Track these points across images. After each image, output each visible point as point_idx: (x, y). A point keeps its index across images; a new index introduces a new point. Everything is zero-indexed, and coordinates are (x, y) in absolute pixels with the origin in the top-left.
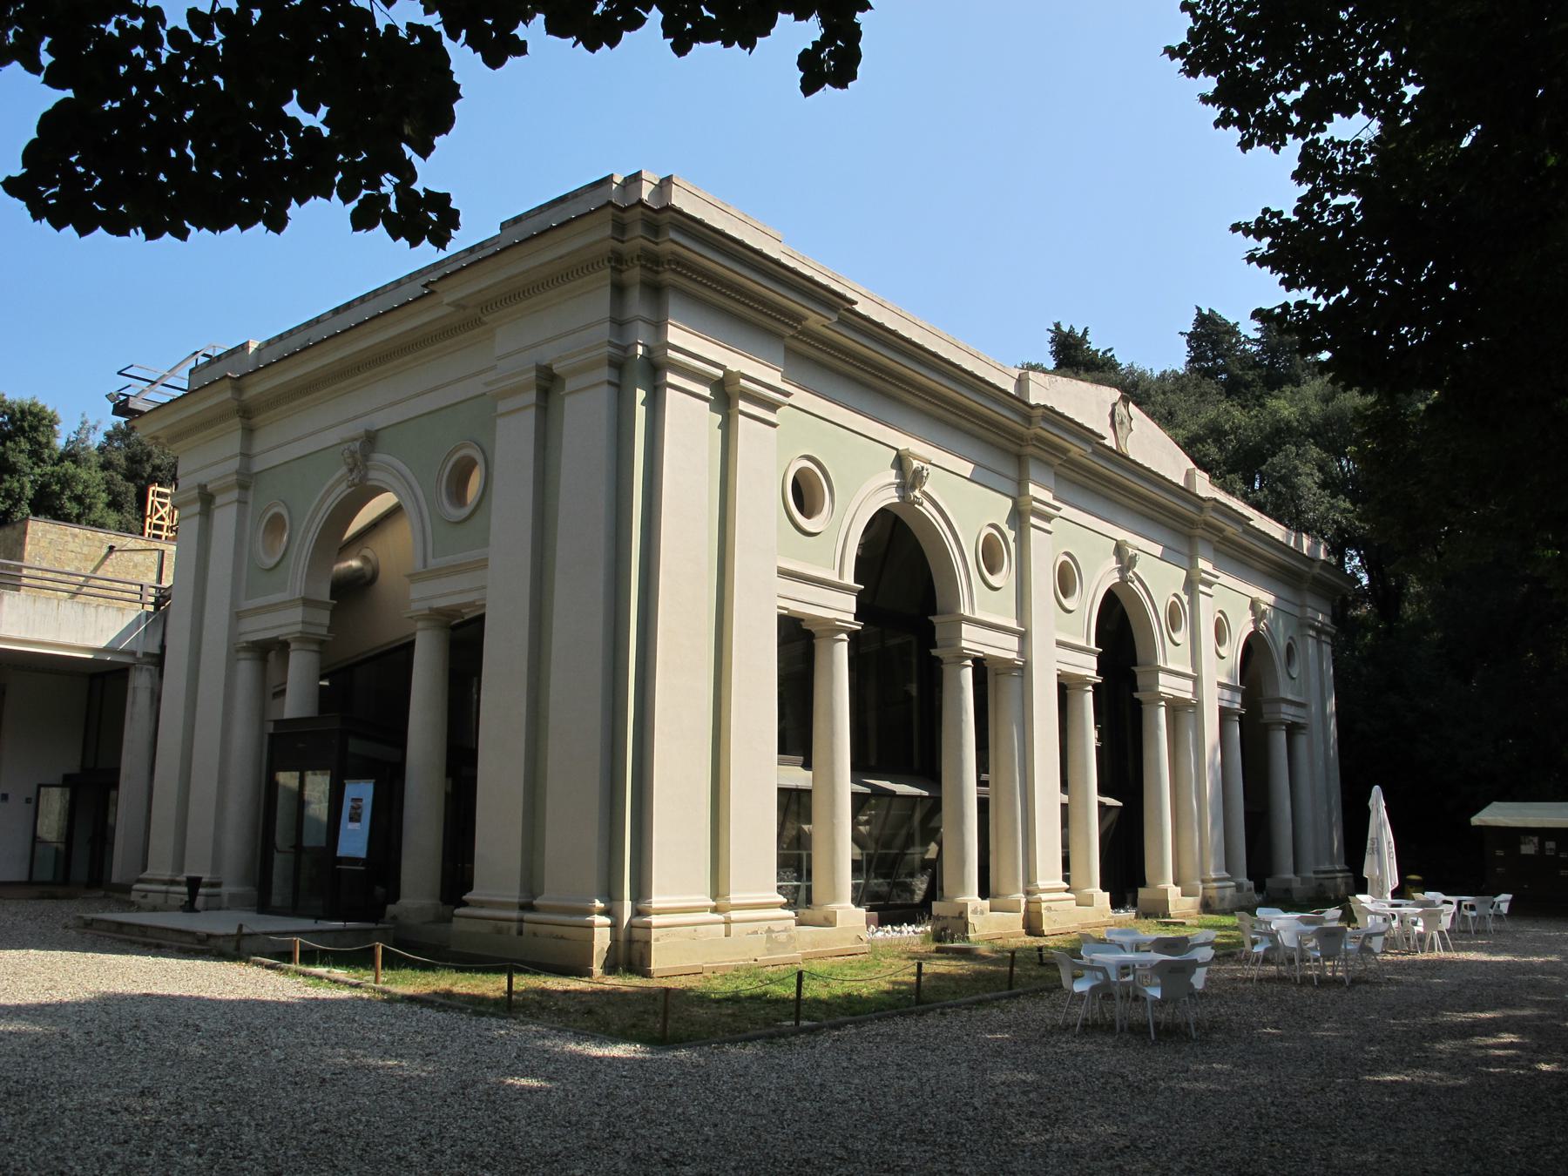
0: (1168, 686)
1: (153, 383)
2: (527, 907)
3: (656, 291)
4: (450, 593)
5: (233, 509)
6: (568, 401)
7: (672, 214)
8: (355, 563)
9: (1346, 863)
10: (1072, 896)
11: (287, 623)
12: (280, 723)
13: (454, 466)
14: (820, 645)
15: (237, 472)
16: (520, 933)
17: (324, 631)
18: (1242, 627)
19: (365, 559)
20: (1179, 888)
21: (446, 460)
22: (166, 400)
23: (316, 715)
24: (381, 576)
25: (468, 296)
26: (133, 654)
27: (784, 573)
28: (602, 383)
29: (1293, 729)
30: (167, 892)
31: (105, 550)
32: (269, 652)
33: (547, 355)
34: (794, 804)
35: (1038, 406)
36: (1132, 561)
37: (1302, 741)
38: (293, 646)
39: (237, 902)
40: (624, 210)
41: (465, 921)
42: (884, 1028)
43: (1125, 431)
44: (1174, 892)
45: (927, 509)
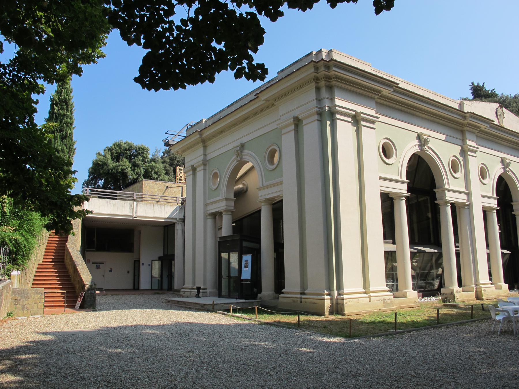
1: (175, 135)
2: (303, 293)
3: (330, 88)
4: (272, 193)
6: (304, 127)
8: (241, 186)
11: (221, 206)
14: (396, 202)
17: (233, 208)
19: (244, 184)
23: (232, 235)
26: (176, 219)
27: (381, 178)
30: (191, 292)
32: (216, 216)
33: (296, 113)
35: (468, 113)
38: (223, 213)
39: (212, 294)
41: (283, 299)
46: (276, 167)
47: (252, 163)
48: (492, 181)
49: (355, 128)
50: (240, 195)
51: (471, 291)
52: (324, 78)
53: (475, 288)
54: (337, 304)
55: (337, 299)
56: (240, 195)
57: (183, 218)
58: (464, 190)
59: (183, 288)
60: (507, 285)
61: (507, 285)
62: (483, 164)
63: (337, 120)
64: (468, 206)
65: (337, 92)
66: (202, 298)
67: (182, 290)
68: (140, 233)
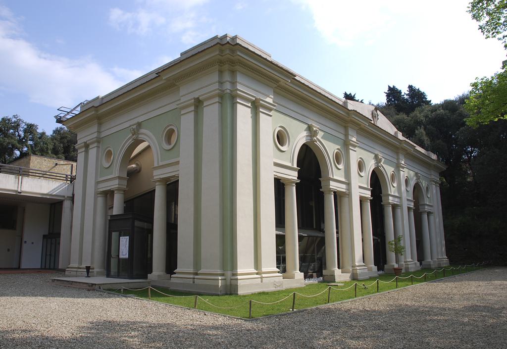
1: (68, 113)
2: (197, 274)
3: (233, 73)
5: (95, 149)
6: (205, 109)
8: (134, 166)
11: (114, 185)
12: (112, 216)
13: (169, 129)
15: (96, 137)
16: (194, 282)
17: (125, 187)
19: (137, 164)
20: (340, 270)
21: (166, 128)
24: (142, 169)
26: (64, 196)
27: (276, 164)
28: (216, 102)
29: (429, 213)
30: (77, 271)
31: (54, 165)
32: (108, 195)
34: (281, 240)
35: (351, 110)
37: (432, 217)
38: (115, 192)
39: (99, 274)
40: (223, 45)
41: (176, 280)
42: (284, 313)
43: (377, 119)
44: (338, 272)
47: (148, 141)
50: (133, 175)
57: (72, 196)
58: (343, 180)
59: (68, 268)
60: (376, 267)
62: (360, 158)
64: (348, 195)
65: (240, 78)
66: (25, 121)
68: (24, 210)
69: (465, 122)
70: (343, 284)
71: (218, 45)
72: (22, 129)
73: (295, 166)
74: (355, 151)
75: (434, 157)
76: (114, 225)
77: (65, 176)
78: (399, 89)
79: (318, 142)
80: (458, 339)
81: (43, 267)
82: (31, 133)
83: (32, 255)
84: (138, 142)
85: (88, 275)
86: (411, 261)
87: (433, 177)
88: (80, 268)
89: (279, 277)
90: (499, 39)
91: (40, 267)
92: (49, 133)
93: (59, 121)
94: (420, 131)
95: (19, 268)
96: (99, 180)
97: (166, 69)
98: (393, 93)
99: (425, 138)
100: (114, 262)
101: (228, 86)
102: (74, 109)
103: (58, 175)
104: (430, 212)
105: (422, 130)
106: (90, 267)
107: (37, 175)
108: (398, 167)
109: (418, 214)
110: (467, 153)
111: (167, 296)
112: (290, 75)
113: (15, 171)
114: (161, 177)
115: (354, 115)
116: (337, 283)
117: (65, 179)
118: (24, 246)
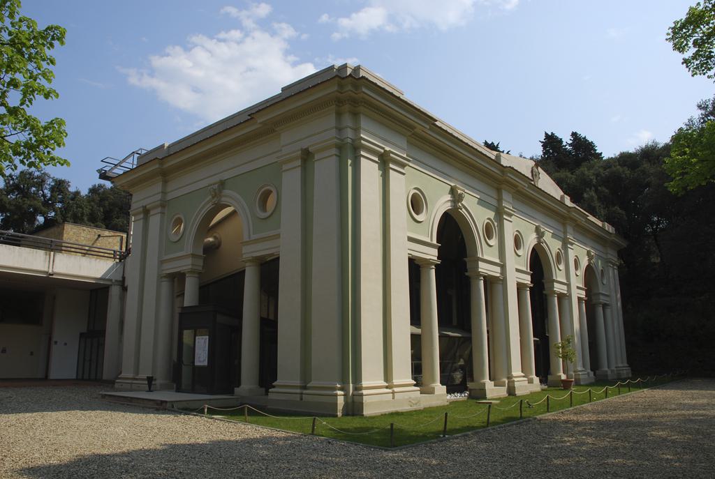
0: (558, 288)
1: (116, 165)
2: (305, 388)
3: (355, 115)
4: (262, 250)
7: (364, 81)
8: (211, 239)
9: (628, 363)
10: (418, 388)
11: (185, 265)
12: (183, 308)
13: (262, 194)
14: (423, 271)
15: (161, 200)
16: (302, 399)
18: (584, 262)
19: (215, 237)
20: (493, 382)
22: (121, 172)
23: (197, 304)
25: (268, 120)
26: (111, 280)
27: (411, 239)
29: (605, 306)
31: (97, 237)
32: (177, 279)
33: (305, 144)
34: (416, 341)
35: (507, 167)
36: (543, 233)
37: (608, 311)
38: (187, 275)
40: (343, 78)
41: (274, 395)
44: (489, 385)
45: (463, 211)
46: (269, 216)
47: (234, 207)
48: (526, 252)
49: (381, 172)
51: (503, 385)
52: (348, 100)
53: (507, 382)
54: (353, 402)
55: (353, 395)
56: (211, 250)
57: (121, 279)
58: (497, 261)
59: (120, 378)
61: (445, 387)
62: (517, 231)
63: (362, 158)
64: (502, 280)
65: (364, 123)
67: (117, 381)
69: (667, 187)
70: (498, 402)
71: (337, 79)
72: (48, 187)
73: (435, 242)
74: (511, 222)
75: (608, 227)
76: (187, 319)
77: (113, 252)
78: (618, 154)
79: (463, 209)
80: (679, 473)
81: (80, 377)
82: (61, 192)
83: (64, 361)
84: (219, 207)
85: (150, 388)
86: (583, 371)
87: (609, 256)
88: (137, 379)
89: (415, 392)
90: (709, 77)
91: (74, 377)
92: (84, 192)
93: (103, 176)
94: (589, 194)
95: (46, 378)
96: (165, 258)
97: (263, 109)
98: (551, 142)
99: (597, 204)
100: (186, 372)
101: (349, 134)
102: (124, 160)
103: (101, 250)
104: (605, 304)
105: (593, 193)
106: (152, 377)
107: (73, 250)
108: (565, 243)
109: (590, 305)
110: (652, 223)
111: (263, 415)
112: (430, 120)
113: (41, 245)
114: (254, 256)
115: (510, 173)
116: (489, 400)
117: (112, 256)
118: (54, 348)
